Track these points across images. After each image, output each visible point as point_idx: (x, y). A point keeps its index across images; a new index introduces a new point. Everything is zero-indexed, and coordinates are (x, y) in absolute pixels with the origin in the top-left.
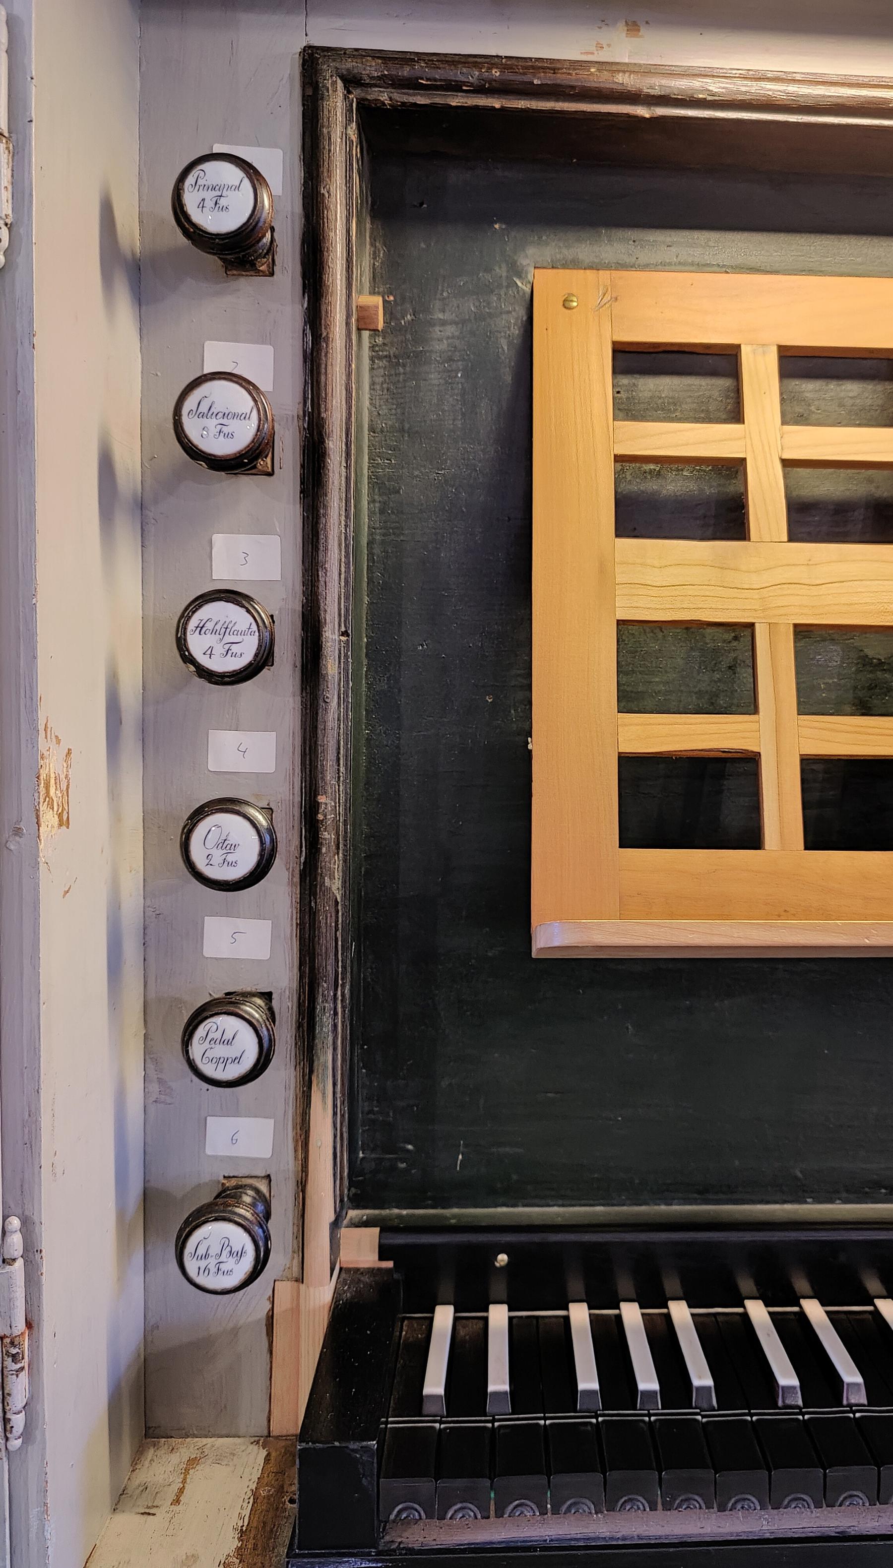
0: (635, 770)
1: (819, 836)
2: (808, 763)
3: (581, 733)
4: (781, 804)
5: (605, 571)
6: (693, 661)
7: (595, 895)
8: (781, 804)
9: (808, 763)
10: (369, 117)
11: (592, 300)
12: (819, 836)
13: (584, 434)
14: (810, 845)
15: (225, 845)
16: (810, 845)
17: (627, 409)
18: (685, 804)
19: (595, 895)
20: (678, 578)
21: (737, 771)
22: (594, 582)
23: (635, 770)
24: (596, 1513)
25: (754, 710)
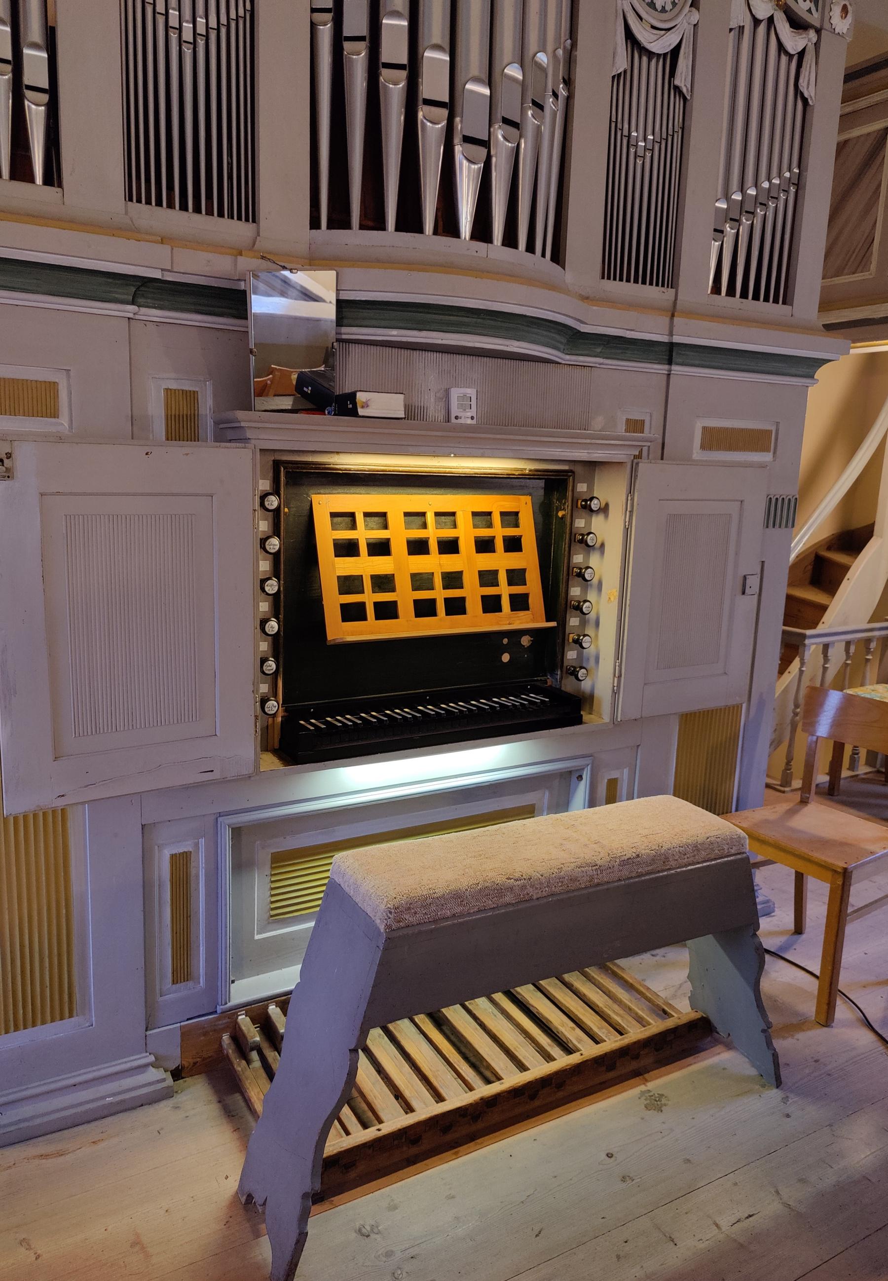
0: (417, 602)
1: (377, 618)
2: (445, 599)
3: (332, 600)
4: (370, 611)
5: (333, 565)
6: (349, 584)
7: (340, 631)
8: (370, 611)
9: (445, 599)
10: (287, 474)
11: (326, 503)
12: (377, 618)
13: (326, 535)
14: (417, 616)
15: (272, 627)
16: (417, 616)
17: (334, 527)
18: (352, 613)
19: (340, 631)
20: (347, 566)
21: (362, 605)
22: (332, 568)
23: (417, 602)
24: (55, 821)
25: (363, 592)
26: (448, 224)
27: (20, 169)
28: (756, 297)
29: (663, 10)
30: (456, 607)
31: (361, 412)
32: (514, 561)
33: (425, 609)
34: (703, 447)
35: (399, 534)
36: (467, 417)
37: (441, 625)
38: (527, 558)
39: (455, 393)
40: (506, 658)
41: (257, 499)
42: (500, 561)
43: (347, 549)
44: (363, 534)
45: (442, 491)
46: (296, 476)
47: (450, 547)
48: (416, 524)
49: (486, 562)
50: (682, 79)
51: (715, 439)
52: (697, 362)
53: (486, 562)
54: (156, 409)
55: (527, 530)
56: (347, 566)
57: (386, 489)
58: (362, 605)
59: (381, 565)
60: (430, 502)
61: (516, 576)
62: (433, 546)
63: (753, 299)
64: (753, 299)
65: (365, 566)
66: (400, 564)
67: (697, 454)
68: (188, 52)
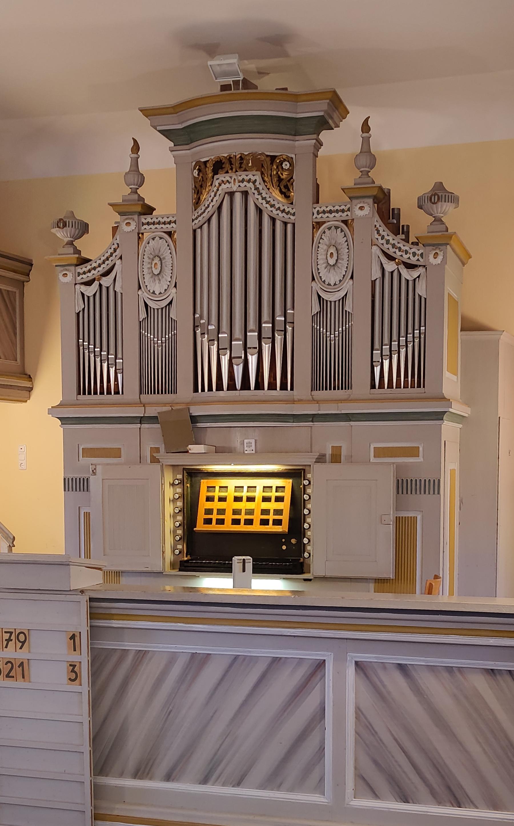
6: (209, 511)
9: (217, 519)
11: (204, 483)
20: (209, 505)
22: (203, 505)
26: (232, 386)
27: (373, 386)
28: (90, 393)
29: (335, 284)
30: (221, 522)
31: (190, 451)
32: (279, 506)
33: (236, 522)
34: (375, 457)
35: (258, 494)
36: (248, 450)
37: (214, 527)
38: (285, 506)
39: (246, 441)
40: (284, 547)
41: (312, 483)
42: (272, 506)
43: (209, 499)
44: (217, 494)
45: (252, 478)
46: (193, 475)
47: (251, 499)
48: (247, 490)
49: (265, 505)
50: (347, 308)
51: (380, 453)
52: (364, 419)
53: (265, 505)
54: (147, 454)
55: (287, 495)
56: (209, 505)
57: (227, 478)
58: (268, 520)
59: (222, 505)
60: (245, 482)
61: (278, 512)
62: (245, 499)
63: (83, 394)
64: (83, 394)
65: (216, 505)
66: (230, 505)
67: (372, 459)
68: (333, 343)
